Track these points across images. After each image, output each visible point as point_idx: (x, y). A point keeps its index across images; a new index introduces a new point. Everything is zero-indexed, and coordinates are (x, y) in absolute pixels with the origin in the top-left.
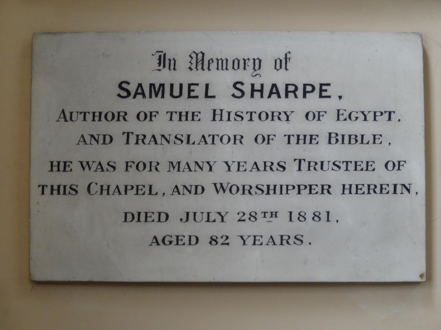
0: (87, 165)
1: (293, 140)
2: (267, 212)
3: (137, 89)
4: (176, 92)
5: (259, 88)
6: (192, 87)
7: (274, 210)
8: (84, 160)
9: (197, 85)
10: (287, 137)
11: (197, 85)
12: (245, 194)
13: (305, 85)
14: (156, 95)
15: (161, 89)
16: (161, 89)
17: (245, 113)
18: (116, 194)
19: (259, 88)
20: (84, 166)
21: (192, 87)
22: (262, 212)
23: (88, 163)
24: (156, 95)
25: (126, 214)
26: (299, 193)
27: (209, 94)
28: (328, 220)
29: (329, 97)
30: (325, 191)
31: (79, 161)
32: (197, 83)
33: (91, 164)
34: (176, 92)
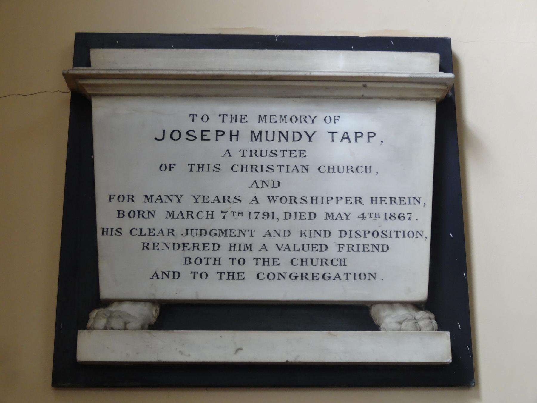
0: (273, 199)
1: (195, 168)
2: (236, 212)
3: (344, 135)
4: (270, 137)
5: (236, 134)
6: (205, 133)
7: (240, 211)
8: (271, 195)
9: (209, 131)
10: (190, 166)
11: (209, 131)
12: (179, 202)
13: (368, 133)
14: (256, 139)
15: (253, 134)
16: (253, 134)
17: (278, 152)
18: (339, 219)
19: (236, 134)
20: (271, 200)
21: (205, 133)
22: (231, 212)
23: (273, 197)
24: (256, 139)
25: (341, 231)
26: (337, 203)
27: (295, 140)
28: (250, 213)
29: (209, 140)
30: (358, 202)
31: (267, 197)
32: (208, 130)
33: (275, 198)
34: (270, 137)
